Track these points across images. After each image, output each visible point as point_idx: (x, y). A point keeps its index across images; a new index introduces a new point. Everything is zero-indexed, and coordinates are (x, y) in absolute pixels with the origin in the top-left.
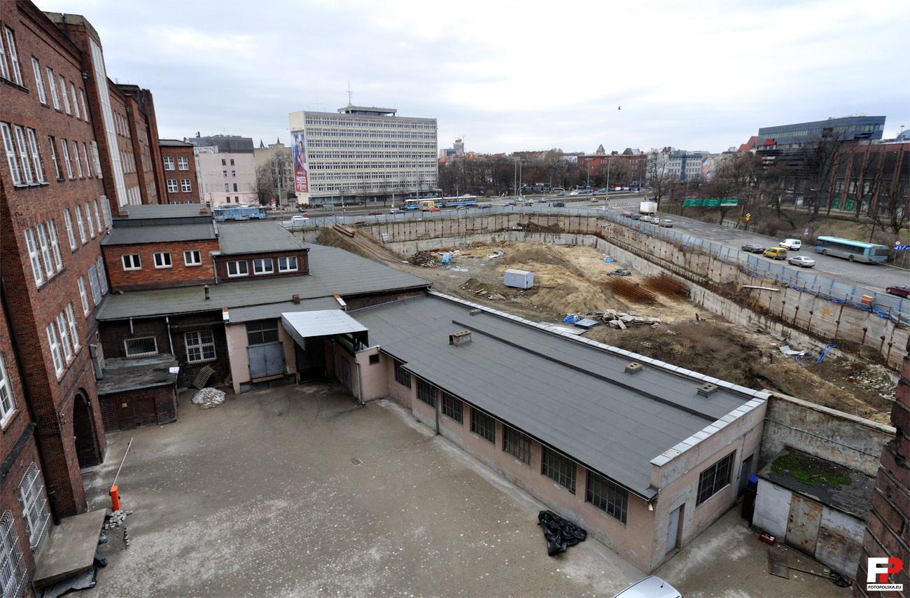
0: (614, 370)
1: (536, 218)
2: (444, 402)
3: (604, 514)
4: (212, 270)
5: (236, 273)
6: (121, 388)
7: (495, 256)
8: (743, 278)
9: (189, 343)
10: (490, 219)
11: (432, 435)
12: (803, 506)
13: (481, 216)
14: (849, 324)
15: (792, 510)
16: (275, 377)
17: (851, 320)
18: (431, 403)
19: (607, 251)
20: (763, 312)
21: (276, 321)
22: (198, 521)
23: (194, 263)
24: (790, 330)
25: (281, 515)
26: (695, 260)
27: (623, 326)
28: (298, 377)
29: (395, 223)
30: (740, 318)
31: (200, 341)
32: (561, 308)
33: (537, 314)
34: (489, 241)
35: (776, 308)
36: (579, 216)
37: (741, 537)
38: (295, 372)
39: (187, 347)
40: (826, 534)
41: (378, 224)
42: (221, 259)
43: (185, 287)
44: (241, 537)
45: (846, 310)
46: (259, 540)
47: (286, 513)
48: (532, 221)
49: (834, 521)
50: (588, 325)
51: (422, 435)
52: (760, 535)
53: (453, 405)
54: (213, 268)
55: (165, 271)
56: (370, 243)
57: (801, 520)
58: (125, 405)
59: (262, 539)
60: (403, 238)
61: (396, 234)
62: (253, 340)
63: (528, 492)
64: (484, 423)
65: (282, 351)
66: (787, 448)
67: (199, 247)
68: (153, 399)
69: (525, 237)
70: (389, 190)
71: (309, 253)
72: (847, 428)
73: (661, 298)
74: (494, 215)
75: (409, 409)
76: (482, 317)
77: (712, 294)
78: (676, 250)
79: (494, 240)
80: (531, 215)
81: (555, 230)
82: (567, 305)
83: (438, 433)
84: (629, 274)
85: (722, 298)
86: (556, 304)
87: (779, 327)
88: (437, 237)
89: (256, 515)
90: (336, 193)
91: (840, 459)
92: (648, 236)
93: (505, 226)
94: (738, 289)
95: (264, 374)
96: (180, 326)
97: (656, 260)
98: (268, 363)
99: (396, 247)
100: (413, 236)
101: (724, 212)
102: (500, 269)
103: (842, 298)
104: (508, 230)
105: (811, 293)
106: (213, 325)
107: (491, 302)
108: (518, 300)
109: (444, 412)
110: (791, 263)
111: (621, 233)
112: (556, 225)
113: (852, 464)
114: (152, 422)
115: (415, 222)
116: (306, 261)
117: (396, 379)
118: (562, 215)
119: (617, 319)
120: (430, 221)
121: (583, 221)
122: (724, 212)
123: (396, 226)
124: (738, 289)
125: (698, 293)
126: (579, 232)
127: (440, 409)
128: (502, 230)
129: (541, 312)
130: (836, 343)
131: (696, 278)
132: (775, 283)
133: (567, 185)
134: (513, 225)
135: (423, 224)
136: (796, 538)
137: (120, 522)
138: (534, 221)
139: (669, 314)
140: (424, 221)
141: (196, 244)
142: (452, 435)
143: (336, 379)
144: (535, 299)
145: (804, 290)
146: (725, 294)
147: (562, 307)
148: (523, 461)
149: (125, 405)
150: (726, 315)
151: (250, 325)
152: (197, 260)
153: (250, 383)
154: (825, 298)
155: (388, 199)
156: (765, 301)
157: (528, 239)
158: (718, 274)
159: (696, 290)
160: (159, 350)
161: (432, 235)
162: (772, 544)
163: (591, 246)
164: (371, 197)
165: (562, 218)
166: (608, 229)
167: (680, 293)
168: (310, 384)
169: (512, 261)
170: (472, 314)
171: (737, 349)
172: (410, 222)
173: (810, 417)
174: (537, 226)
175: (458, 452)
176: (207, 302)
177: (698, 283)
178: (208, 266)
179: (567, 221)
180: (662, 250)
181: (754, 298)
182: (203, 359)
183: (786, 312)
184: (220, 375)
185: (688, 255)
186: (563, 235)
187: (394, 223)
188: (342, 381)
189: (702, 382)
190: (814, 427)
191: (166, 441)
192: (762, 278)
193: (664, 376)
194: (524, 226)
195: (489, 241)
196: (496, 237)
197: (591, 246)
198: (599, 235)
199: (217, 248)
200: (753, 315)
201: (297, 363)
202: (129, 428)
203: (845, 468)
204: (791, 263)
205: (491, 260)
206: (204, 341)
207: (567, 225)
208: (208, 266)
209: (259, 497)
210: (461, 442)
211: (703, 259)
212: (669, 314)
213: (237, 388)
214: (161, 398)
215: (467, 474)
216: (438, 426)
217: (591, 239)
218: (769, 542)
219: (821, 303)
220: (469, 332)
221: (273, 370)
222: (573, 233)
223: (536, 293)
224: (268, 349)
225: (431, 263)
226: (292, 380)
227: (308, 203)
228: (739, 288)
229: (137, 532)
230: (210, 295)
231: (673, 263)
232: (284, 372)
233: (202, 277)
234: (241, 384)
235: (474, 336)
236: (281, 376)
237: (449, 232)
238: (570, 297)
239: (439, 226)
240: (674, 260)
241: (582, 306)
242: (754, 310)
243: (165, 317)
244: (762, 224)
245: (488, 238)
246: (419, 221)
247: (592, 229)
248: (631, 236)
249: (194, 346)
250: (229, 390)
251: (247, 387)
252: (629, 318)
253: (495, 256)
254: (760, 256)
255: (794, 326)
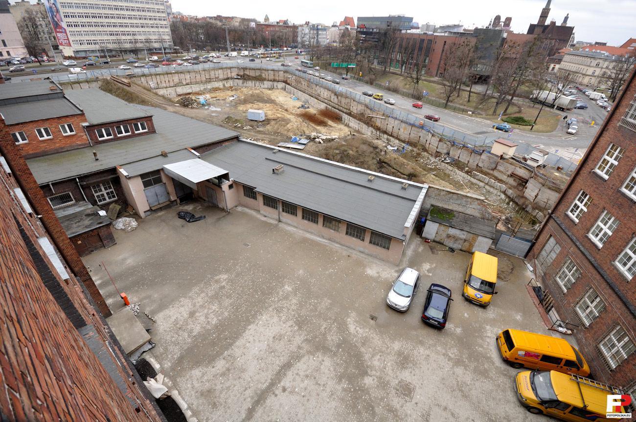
0: (362, 180)
1: (248, 70)
2: (283, 206)
3: (378, 248)
4: (85, 137)
5: (104, 137)
6: (73, 233)
7: (233, 98)
8: (369, 111)
9: (96, 192)
10: (220, 71)
11: (277, 223)
12: (442, 228)
13: (214, 69)
14: (414, 134)
15: (438, 230)
16: (165, 204)
17: (415, 132)
18: (275, 207)
19: (292, 92)
20: (378, 129)
21: (158, 172)
22: (185, 297)
23: (69, 133)
24: (390, 138)
25: (228, 282)
26: (343, 100)
27: (322, 142)
28: (178, 201)
29: (157, 74)
30: (368, 132)
31: (103, 189)
32: (285, 133)
33: (276, 137)
34: (221, 87)
35: (383, 127)
36: (273, 70)
37: (419, 242)
38: (176, 198)
39: (95, 195)
40: (449, 236)
41: (144, 75)
42: (90, 128)
43: (68, 151)
44: (217, 298)
45: (413, 128)
46: (227, 298)
47: (230, 280)
48: (245, 72)
49: (452, 231)
50: (305, 143)
51: (271, 224)
52: (426, 240)
53: (290, 208)
54: (86, 135)
55: (49, 141)
56: (146, 91)
57: (441, 232)
58: (80, 242)
59: (229, 297)
60: (165, 85)
61: (159, 83)
62: (146, 184)
63: (337, 243)
64: (311, 215)
65: (166, 188)
66: (432, 205)
67: (71, 121)
68: (98, 234)
69: (243, 83)
70: (139, 45)
71: (153, 118)
72: (455, 196)
73: (330, 122)
74: (222, 68)
75: (258, 211)
76: (280, 154)
77: (353, 119)
78: (333, 95)
79: (224, 85)
80: (245, 69)
81: (260, 79)
82: (288, 130)
83: (280, 221)
84: (308, 108)
85: (358, 122)
86: (282, 130)
87: (386, 136)
88: (187, 84)
89: (215, 286)
90: (97, 47)
91: (450, 208)
92: (316, 85)
93: (229, 76)
94: (366, 117)
95: (157, 203)
96: (88, 182)
97: (322, 100)
98: (159, 197)
99: (161, 92)
100: (172, 84)
101: (348, 70)
102: (241, 108)
103: (412, 122)
104: (232, 78)
105: (399, 120)
106: (112, 177)
107: (245, 131)
108: (261, 129)
109: (283, 211)
110: (385, 102)
111: (300, 82)
112: (260, 76)
113: (454, 209)
114: (101, 247)
115: (171, 73)
116: (152, 124)
117: (245, 195)
118: (263, 70)
119: (318, 138)
120: (181, 73)
121: (276, 73)
122: (348, 70)
123: (158, 77)
124: (366, 117)
125: (346, 118)
126: (274, 80)
127: (281, 210)
128: (228, 79)
129: (277, 136)
130: (409, 143)
131: (345, 111)
132: (383, 115)
133: (255, 45)
134: (234, 75)
135: (177, 75)
136: (437, 239)
137: (138, 311)
138: (247, 72)
139: (336, 132)
140: (177, 73)
141: (68, 119)
142: (289, 222)
143: (201, 198)
144: (269, 127)
145: (396, 119)
146: (360, 120)
147: (286, 132)
148: (335, 230)
149: (80, 242)
150: (360, 130)
151: (142, 176)
152: (71, 131)
153: (151, 210)
154: (406, 123)
155: (139, 53)
156: (378, 123)
157: (245, 84)
158: (356, 109)
159: (345, 117)
160: (76, 200)
161: (184, 83)
162: (429, 242)
163: (282, 89)
164: (126, 51)
165: (264, 71)
166: (292, 79)
167: (337, 119)
168: (187, 204)
169: (245, 102)
170: (275, 153)
171: (372, 149)
172: (167, 74)
173: (442, 193)
174: (249, 76)
175: (295, 229)
176: (98, 163)
177: (346, 113)
178: (82, 134)
179: (266, 73)
180: (325, 94)
181: (373, 122)
182: (108, 200)
183: (388, 129)
184: (125, 206)
185: (339, 98)
186: (265, 82)
187: (156, 75)
188: (207, 199)
189: (402, 183)
190: (443, 197)
191: (121, 257)
192: (377, 112)
193: (384, 180)
194: (241, 76)
195: (221, 87)
196: (225, 83)
197: (282, 89)
198: (286, 82)
199: (85, 121)
200: (374, 131)
201: (176, 194)
202: (87, 255)
203: (452, 210)
204: (385, 102)
205: (231, 101)
206: (106, 189)
207: (267, 75)
208: (82, 134)
209: (209, 276)
210: (295, 224)
211: (348, 100)
212: (336, 132)
213: (142, 214)
214: (103, 233)
215: (305, 240)
216: (279, 218)
217: (281, 85)
218: (429, 242)
219: (403, 125)
220: (282, 166)
221: (163, 200)
222: (271, 81)
223: (269, 124)
224: (157, 189)
225: (195, 105)
226: (175, 203)
227: (73, 55)
228: (366, 116)
229: (154, 312)
230: (98, 157)
231: (330, 101)
232: (169, 200)
233: (79, 143)
234: (145, 212)
235: (286, 168)
236: (168, 203)
237: (195, 80)
238: (288, 126)
239: (188, 76)
240: (332, 100)
241: (297, 131)
242: (374, 128)
243: (75, 179)
244: (367, 78)
245: (220, 85)
246: (174, 73)
247: (281, 78)
248: (306, 84)
249: (99, 193)
250: (136, 215)
251: (149, 213)
252: (324, 138)
253: (233, 98)
254: (371, 98)
255: (391, 136)
